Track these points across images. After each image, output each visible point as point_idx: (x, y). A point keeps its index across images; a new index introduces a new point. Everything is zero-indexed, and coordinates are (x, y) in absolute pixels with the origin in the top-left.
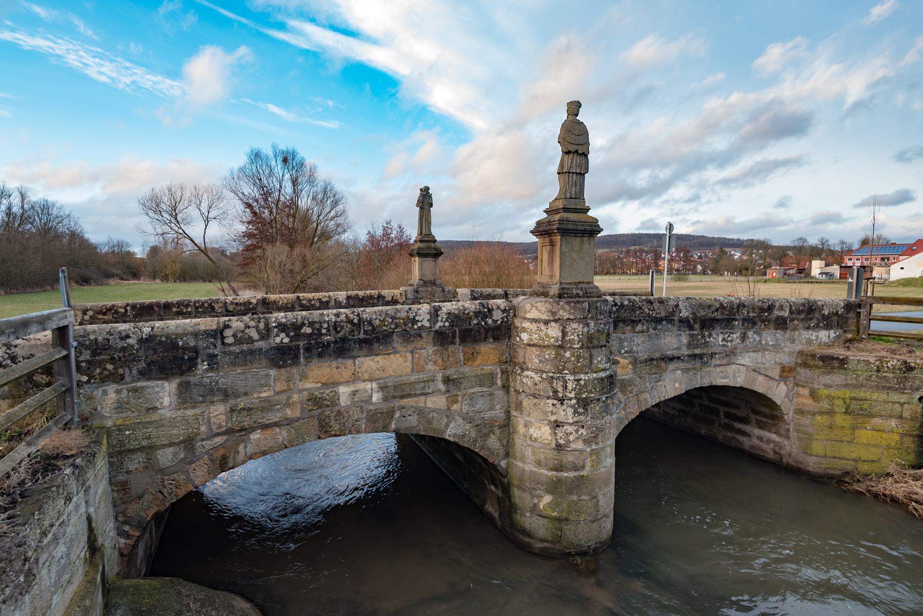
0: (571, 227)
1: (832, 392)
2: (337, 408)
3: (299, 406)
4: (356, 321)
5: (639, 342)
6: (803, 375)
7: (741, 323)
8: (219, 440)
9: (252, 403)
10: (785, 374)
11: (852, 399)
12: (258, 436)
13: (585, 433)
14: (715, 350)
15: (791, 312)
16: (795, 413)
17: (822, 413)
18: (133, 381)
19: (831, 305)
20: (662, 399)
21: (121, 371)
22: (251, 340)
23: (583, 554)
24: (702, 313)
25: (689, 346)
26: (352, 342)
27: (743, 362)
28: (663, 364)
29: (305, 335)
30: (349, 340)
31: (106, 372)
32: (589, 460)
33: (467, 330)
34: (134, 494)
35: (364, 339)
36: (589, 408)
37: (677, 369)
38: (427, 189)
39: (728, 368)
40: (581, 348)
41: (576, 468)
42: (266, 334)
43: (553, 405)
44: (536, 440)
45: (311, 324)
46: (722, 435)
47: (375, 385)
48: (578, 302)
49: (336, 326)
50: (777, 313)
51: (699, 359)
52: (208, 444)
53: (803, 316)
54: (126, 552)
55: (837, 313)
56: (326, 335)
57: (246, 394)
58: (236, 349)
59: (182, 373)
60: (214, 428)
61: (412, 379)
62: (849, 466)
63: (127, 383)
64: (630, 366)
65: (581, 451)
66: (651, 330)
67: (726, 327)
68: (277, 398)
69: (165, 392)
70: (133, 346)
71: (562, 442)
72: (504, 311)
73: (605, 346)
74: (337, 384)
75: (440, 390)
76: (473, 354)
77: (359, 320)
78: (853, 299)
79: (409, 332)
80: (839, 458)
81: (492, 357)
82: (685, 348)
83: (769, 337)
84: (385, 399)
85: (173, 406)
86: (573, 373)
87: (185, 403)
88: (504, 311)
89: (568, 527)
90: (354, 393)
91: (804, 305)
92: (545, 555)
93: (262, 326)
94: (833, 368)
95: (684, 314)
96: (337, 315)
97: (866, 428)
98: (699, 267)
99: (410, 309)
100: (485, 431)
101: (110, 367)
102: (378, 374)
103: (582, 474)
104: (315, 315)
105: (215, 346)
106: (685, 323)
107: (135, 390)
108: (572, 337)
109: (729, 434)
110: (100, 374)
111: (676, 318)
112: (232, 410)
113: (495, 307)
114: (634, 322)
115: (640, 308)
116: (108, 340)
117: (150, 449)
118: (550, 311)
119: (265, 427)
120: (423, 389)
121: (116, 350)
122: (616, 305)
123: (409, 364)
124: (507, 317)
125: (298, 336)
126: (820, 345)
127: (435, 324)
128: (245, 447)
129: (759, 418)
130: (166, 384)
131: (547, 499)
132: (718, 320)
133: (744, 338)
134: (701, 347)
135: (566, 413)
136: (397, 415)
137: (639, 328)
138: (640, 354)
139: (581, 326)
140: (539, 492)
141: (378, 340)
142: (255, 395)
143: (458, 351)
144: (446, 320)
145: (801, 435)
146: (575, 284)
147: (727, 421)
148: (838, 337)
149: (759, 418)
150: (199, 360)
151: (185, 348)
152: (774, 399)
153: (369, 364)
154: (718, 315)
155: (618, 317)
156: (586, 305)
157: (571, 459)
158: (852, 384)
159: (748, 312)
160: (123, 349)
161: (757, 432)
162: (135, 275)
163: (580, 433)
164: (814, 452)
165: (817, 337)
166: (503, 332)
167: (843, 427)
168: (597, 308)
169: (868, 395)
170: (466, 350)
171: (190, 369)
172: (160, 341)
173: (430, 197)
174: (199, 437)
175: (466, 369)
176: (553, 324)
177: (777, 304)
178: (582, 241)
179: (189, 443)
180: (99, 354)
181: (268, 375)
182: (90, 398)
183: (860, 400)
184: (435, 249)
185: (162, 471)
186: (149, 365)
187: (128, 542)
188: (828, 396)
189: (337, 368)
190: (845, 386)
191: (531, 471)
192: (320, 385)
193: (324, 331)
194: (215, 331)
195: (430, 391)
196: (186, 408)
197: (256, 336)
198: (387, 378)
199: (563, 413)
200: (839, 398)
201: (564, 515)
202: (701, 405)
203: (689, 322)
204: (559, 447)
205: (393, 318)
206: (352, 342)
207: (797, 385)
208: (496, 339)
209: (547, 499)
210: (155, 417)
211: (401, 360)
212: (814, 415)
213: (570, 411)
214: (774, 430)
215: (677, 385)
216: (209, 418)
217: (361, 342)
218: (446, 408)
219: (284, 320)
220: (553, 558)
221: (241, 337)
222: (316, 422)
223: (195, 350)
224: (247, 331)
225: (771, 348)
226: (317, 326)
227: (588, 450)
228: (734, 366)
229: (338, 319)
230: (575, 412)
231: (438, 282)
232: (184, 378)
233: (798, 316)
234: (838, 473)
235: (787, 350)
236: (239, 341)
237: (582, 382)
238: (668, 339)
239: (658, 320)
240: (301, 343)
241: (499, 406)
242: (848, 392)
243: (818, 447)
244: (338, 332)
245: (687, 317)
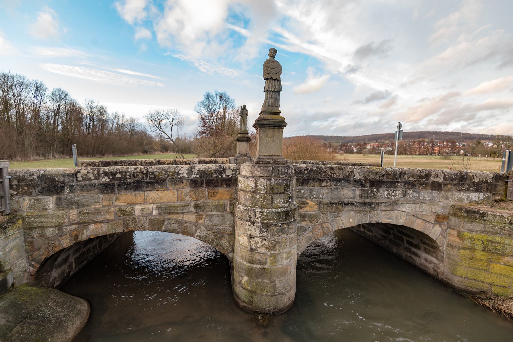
0: (265, 123)
1: (473, 235)
2: (133, 216)
3: (113, 214)
4: (145, 172)
5: (324, 193)
6: (454, 222)
7: (403, 184)
8: (74, 227)
9: (91, 210)
10: (440, 220)
11: (489, 241)
12: (93, 227)
13: (267, 243)
14: (381, 200)
15: (445, 179)
16: (447, 246)
17: (465, 249)
18: (36, 196)
19: (481, 176)
20: (340, 228)
21: (31, 190)
22: (90, 179)
23: (265, 314)
24: (371, 177)
25: (361, 197)
26: (143, 183)
27: (404, 210)
28: (340, 206)
29: (117, 178)
30: (142, 182)
31: (24, 191)
32: (269, 259)
33: (210, 180)
34: (36, 247)
35: (150, 182)
36: (269, 229)
37: (351, 210)
38: (245, 106)
39: (392, 213)
40: (266, 193)
41: (261, 263)
42: (98, 177)
43: (249, 225)
44: (241, 244)
45: (121, 173)
46: (405, 254)
47: (155, 206)
48: (266, 167)
49: (134, 174)
50: (432, 179)
51: (368, 205)
52: (69, 228)
53: (456, 182)
54: (33, 274)
55: (486, 182)
56: (129, 179)
57: (88, 206)
58: (83, 183)
59: (58, 193)
60: (71, 221)
61: (176, 204)
62: (485, 287)
63: (33, 196)
64: (316, 207)
65: (264, 254)
66: (333, 186)
67: (391, 186)
68: (103, 209)
69: (50, 202)
70: (35, 179)
71: (253, 247)
72: (233, 170)
73: (283, 193)
74: (135, 204)
75: (192, 212)
76: (214, 193)
77: (147, 172)
78: (505, 172)
79: (176, 180)
80: (477, 281)
81: (226, 196)
82: (358, 198)
83: (426, 194)
84: (160, 214)
85: (54, 209)
86: (261, 208)
87: (59, 207)
88: (233, 170)
89: (256, 297)
90: (143, 209)
91: (456, 175)
92: (244, 310)
93: (96, 172)
94: (475, 219)
95: (358, 177)
96: (135, 169)
97: (499, 263)
98: (462, 151)
99: (177, 167)
100: (219, 236)
101: (26, 188)
102: (158, 200)
103: (264, 267)
104: (124, 168)
105: (73, 181)
106: (358, 183)
107: (37, 200)
108: (260, 187)
109: (408, 254)
110: (22, 191)
111: (352, 179)
112: (80, 213)
113: (227, 168)
114: (321, 181)
115: (325, 172)
116: (24, 176)
117: (42, 228)
118: (251, 171)
119: (96, 223)
120: (183, 210)
121: (28, 180)
122: (307, 169)
123: (176, 196)
124: (235, 174)
125: (114, 178)
126: (470, 202)
127: (190, 175)
128: (87, 231)
129: (426, 247)
130: (51, 198)
131: (246, 279)
132: (384, 182)
133: (405, 194)
134: (370, 198)
135: (255, 231)
136: (166, 223)
137: (324, 184)
138: (324, 200)
139: (266, 180)
140: (242, 274)
141: (157, 183)
142: (93, 207)
143: (205, 191)
144: (197, 174)
145: (451, 261)
146: (269, 156)
147: (408, 246)
148: (488, 198)
149: (426, 247)
150: (66, 188)
151: (59, 182)
152: (430, 235)
153: (153, 195)
154: (384, 179)
155: (309, 177)
156: (271, 168)
157: (258, 257)
158: (489, 231)
159: (409, 178)
160: (31, 180)
161: (424, 255)
162: (167, 150)
163: (263, 243)
164: (458, 274)
165: (468, 197)
166: (232, 182)
167: (481, 260)
168: (279, 171)
169: (502, 240)
170: (210, 191)
171: (61, 192)
172: (47, 177)
173: (247, 110)
174: (64, 225)
175: (210, 202)
176: (251, 179)
177: (433, 174)
178: (274, 131)
179: (60, 227)
180: (21, 182)
181: (99, 197)
182: (18, 202)
183: (495, 243)
184: (247, 138)
185: (48, 238)
186: (43, 188)
187: (34, 269)
188: (470, 238)
189: (135, 196)
190: (484, 232)
191: (239, 262)
192: (126, 204)
193: (128, 177)
194: (73, 174)
195: (186, 211)
196: (59, 210)
197: (93, 178)
198: (162, 203)
199: (254, 231)
200: (478, 239)
201: (254, 289)
202: (394, 234)
203: (361, 182)
204: (252, 250)
205: (166, 171)
206: (143, 183)
207: (450, 228)
208: (228, 185)
209: (246, 279)
210: (45, 213)
211: (171, 194)
212: (459, 249)
213: (258, 230)
214: (434, 255)
215: (351, 220)
216: (69, 216)
217: (148, 183)
218: (195, 221)
219: (107, 170)
220: (248, 313)
221: (85, 178)
222: (122, 222)
223: (64, 183)
224: (88, 175)
225: (428, 202)
226: (124, 174)
227: (269, 253)
228: (396, 212)
229: (136, 171)
230: (261, 230)
231: (248, 155)
232: (59, 196)
233: (451, 182)
234: (476, 290)
235: (441, 204)
236: (84, 179)
237: (265, 214)
238: (345, 192)
239: (338, 180)
240: (116, 182)
241: (228, 223)
242: (486, 236)
243: (461, 271)
244: (135, 178)
245: (360, 179)
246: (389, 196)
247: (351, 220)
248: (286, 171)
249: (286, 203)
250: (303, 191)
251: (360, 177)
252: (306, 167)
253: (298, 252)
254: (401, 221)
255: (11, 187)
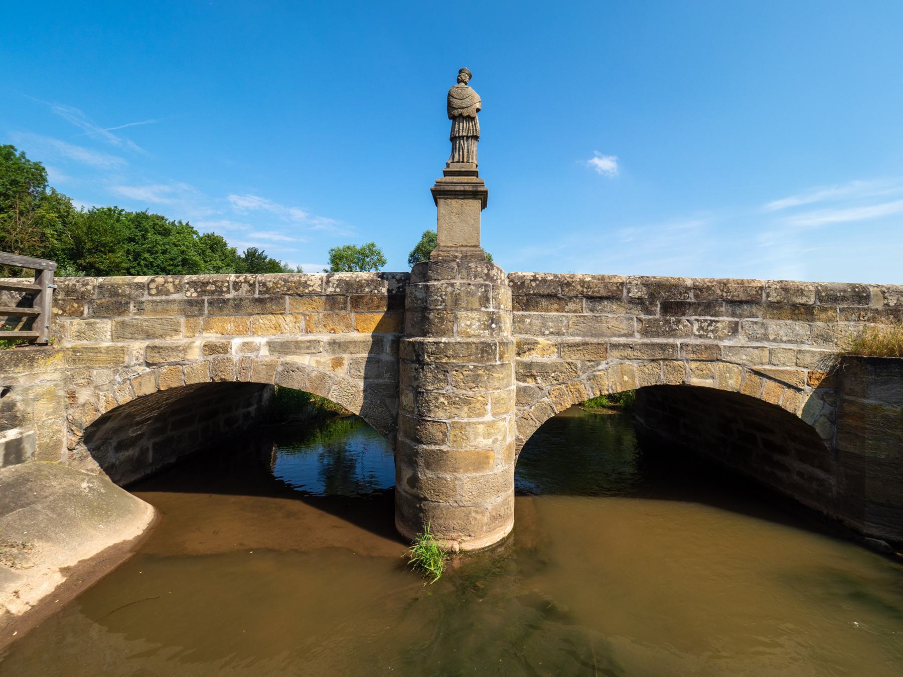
18: (89, 318)
43: (416, 369)
59: (120, 314)
116: (75, 285)
137: (571, 306)
144: (337, 286)
193: (225, 289)
197: (171, 289)
205: (285, 281)
228: (721, 364)
240: (206, 298)
246: (702, 332)
247: (626, 378)
248: (486, 271)
249: (484, 329)
250: (528, 321)
251: (639, 294)
252: (534, 276)
253: (521, 437)
254: (731, 381)
255: (55, 302)
